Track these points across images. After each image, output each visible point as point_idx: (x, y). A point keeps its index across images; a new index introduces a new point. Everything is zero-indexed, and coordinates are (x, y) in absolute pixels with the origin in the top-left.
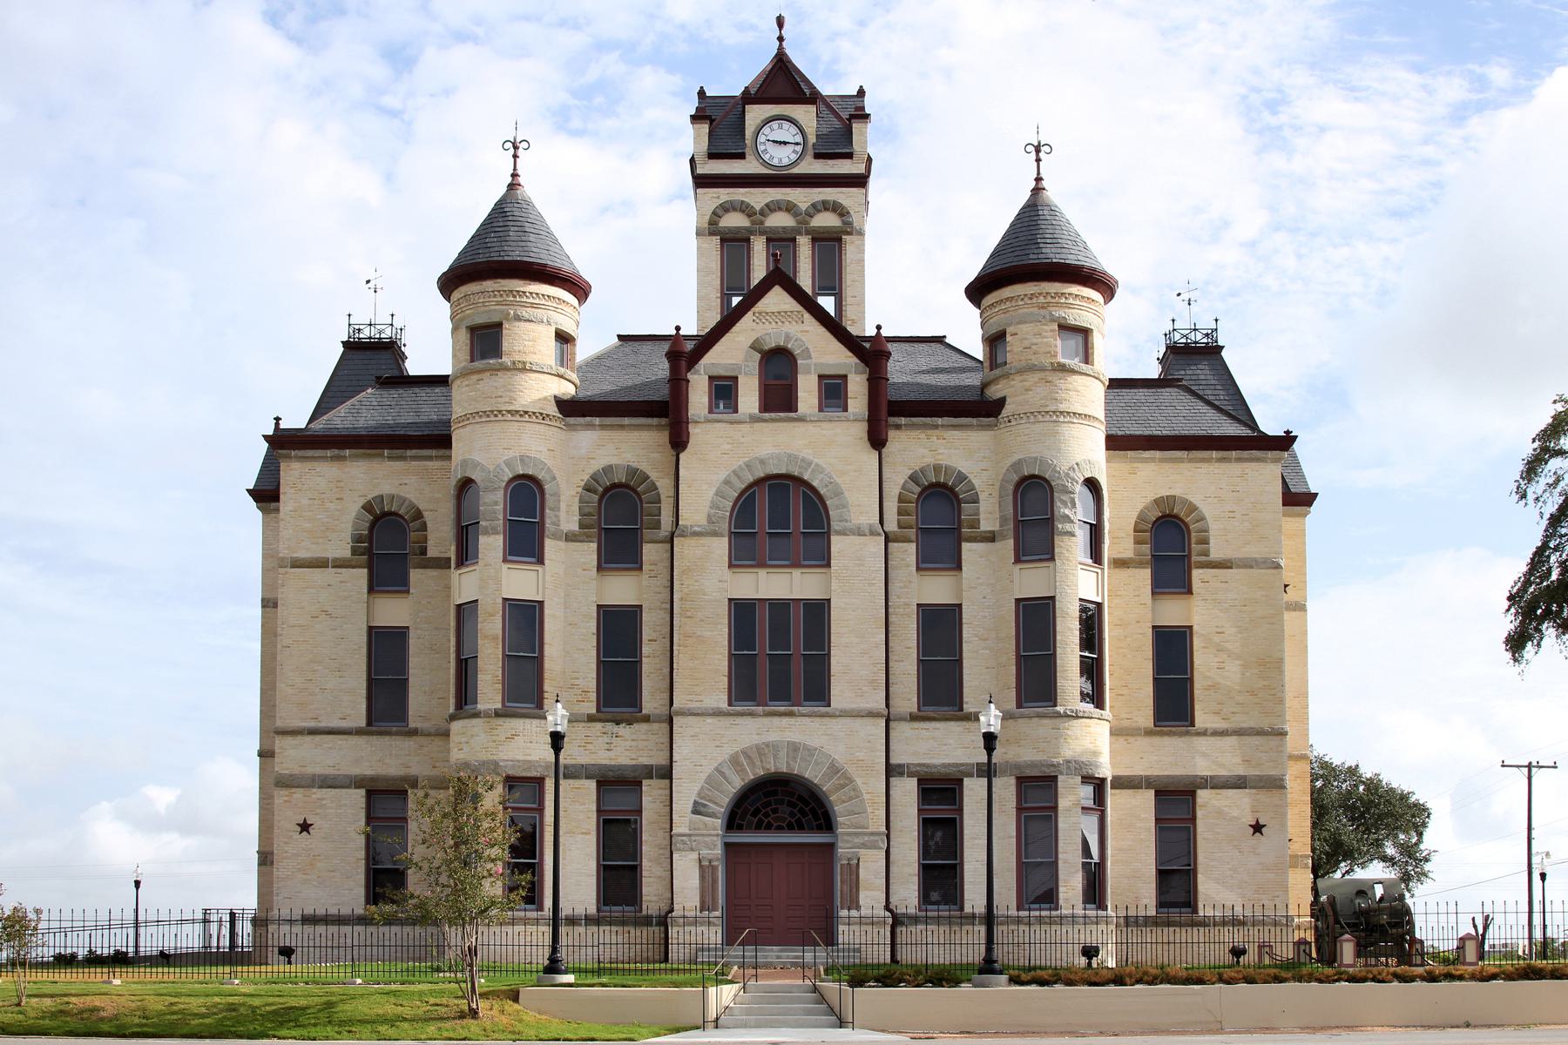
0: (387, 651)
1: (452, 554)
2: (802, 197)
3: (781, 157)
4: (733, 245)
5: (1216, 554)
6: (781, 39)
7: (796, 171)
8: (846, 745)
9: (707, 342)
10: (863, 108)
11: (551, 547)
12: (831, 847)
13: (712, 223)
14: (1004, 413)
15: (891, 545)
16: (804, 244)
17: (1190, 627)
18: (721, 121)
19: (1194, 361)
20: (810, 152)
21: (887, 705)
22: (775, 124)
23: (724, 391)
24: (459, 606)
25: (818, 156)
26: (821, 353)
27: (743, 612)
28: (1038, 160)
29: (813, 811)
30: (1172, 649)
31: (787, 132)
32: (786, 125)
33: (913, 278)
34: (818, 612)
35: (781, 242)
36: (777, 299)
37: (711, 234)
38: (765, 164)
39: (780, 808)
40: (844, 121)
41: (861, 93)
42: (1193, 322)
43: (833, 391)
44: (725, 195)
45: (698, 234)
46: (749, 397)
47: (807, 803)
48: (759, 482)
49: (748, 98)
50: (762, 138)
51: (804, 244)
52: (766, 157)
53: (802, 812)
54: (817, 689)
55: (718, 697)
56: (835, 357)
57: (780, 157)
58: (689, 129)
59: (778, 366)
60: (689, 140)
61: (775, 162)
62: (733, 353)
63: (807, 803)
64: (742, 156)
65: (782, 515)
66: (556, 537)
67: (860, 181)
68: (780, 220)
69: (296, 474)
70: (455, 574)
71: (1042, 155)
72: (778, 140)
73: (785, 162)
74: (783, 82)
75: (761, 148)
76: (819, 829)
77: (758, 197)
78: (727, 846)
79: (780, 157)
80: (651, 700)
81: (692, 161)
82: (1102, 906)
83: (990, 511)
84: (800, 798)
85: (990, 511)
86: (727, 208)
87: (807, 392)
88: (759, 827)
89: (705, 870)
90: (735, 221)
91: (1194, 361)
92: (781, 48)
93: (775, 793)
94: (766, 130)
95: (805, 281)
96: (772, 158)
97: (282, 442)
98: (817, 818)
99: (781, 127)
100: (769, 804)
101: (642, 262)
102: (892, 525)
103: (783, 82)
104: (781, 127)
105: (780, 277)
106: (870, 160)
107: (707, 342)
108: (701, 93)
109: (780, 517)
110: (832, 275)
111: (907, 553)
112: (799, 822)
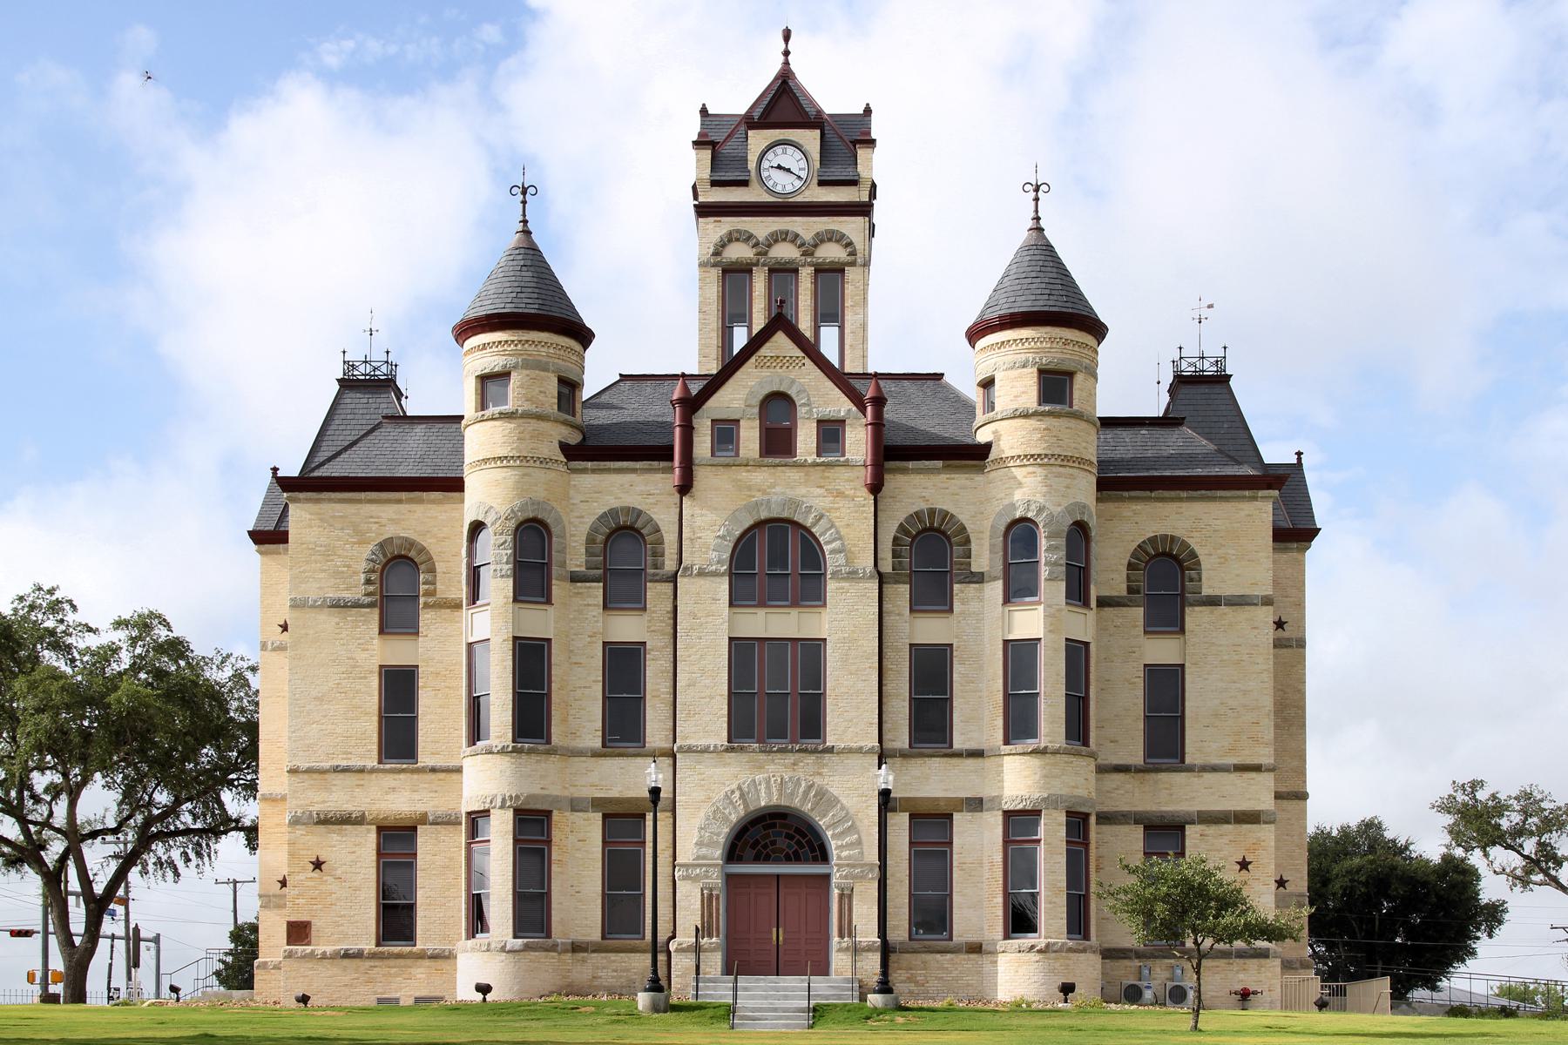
0: (399, 687)
1: (463, 593)
2: (806, 227)
3: (784, 184)
4: (733, 276)
5: (1206, 591)
6: (786, 53)
7: (799, 199)
8: (846, 790)
9: (714, 383)
10: (869, 133)
11: (558, 589)
12: (827, 877)
13: (716, 253)
14: (992, 456)
15: (888, 588)
16: (806, 274)
17: (381, 667)
18: (719, 142)
19: (1202, 391)
20: (815, 181)
21: (880, 741)
22: (779, 149)
23: (726, 433)
24: (470, 645)
25: (821, 183)
26: (820, 400)
27: (741, 649)
28: (1037, 199)
29: (809, 843)
30: (1165, 687)
31: (790, 158)
32: (790, 149)
33: (919, 303)
34: (813, 650)
35: (783, 273)
36: (781, 341)
37: (715, 265)
38: (770, 191)
39: (775, 839)
40: (846, 139)
41: (868, 111)
42: (1201, 349)
43: (831, 433)
44: (729, 223)
45: (701, 265)
46: (750, 438)
47: (804, 836)
48: (760, 524)
49: (751, 122)
50: (765, 164)
51: (806, 274)
52: (770, 184)
53: (798, 843)
54: (811, 724)
55: (718, 734)
56: (838, 404)
57: (789, 179)
58: (692, 154)
59: (777, 407)
60: (690, 166)
61: (779, 189)
62: (737, 398)
63: (804, 836)
64: (744, 183)
65: (776, 559)
66: (560, 578)
67: (864, 210)
68: (785, 252)
69: (303, 516)
70: (465, 612)
71: (1040, 194)
72: (787, 166)
73: (789, 189)
74: (784, 104)
75: (765, 174)
76: (815, 860)
77: (762, 227)
78: (730, 879)
79: (789, 179)
80: (655, 733)
81: (694, 188)
82: (1087, 937)
83: (985, 555)
84: (798, 831)
85: (985, 555)
86: (731, 238)
87: (806, 439)
88: (757, 859)
89: (708, 900)
90: (739, 252)
91: (1202, 391)
92: (787, 63)
93: (774, 825)
94: (770, 155)
95: (805, 324)
96: (776, 184)
97: (286, 484)
98: (813, 850)
99: (785, 153)
100: (768, 836)
101: (649, 315)
102: (887, 566)
103: (784, 104)
104: (785, 153)
105: (780, 322)
106: (874, 186)
107: (714, 383)
108: (704, 111)
109: (778, 557)
110: (830, 312)
111: (901, 594)
112: (796, 853)
